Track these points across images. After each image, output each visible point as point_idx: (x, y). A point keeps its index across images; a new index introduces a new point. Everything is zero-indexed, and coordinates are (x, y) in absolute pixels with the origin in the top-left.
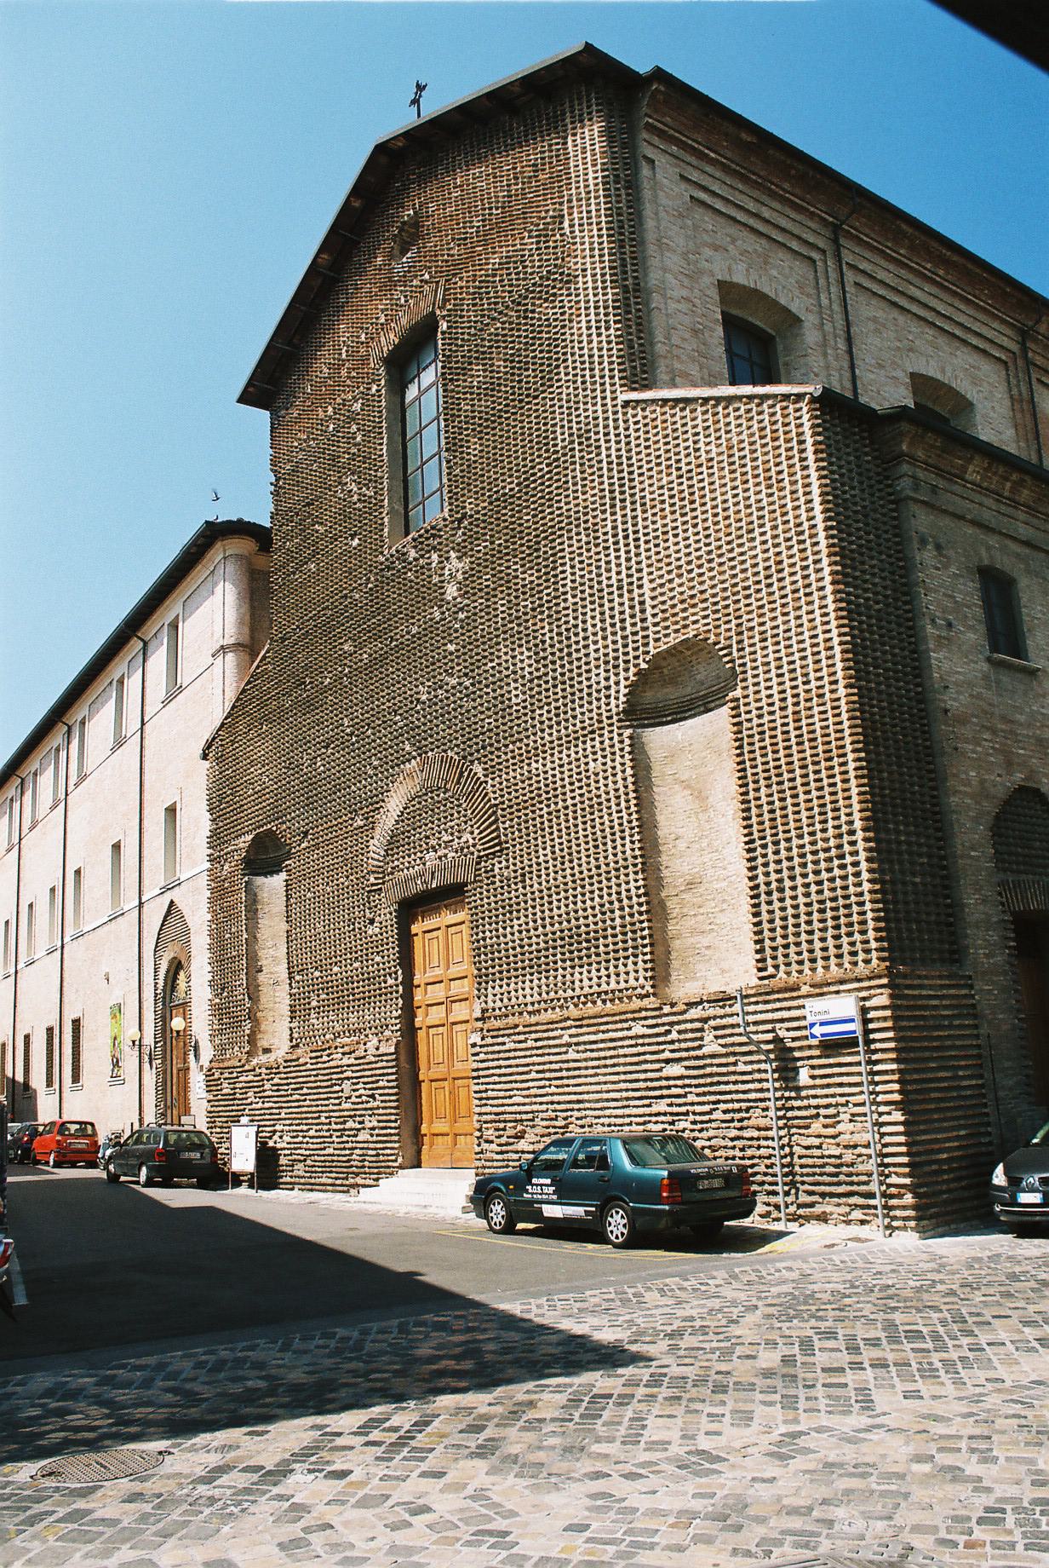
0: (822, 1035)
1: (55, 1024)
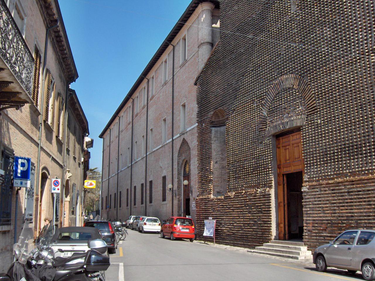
1: (107, 196)
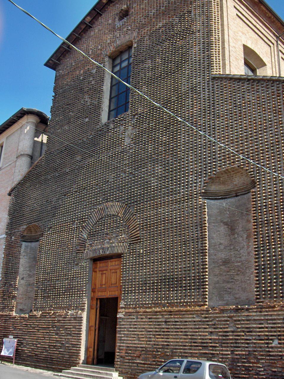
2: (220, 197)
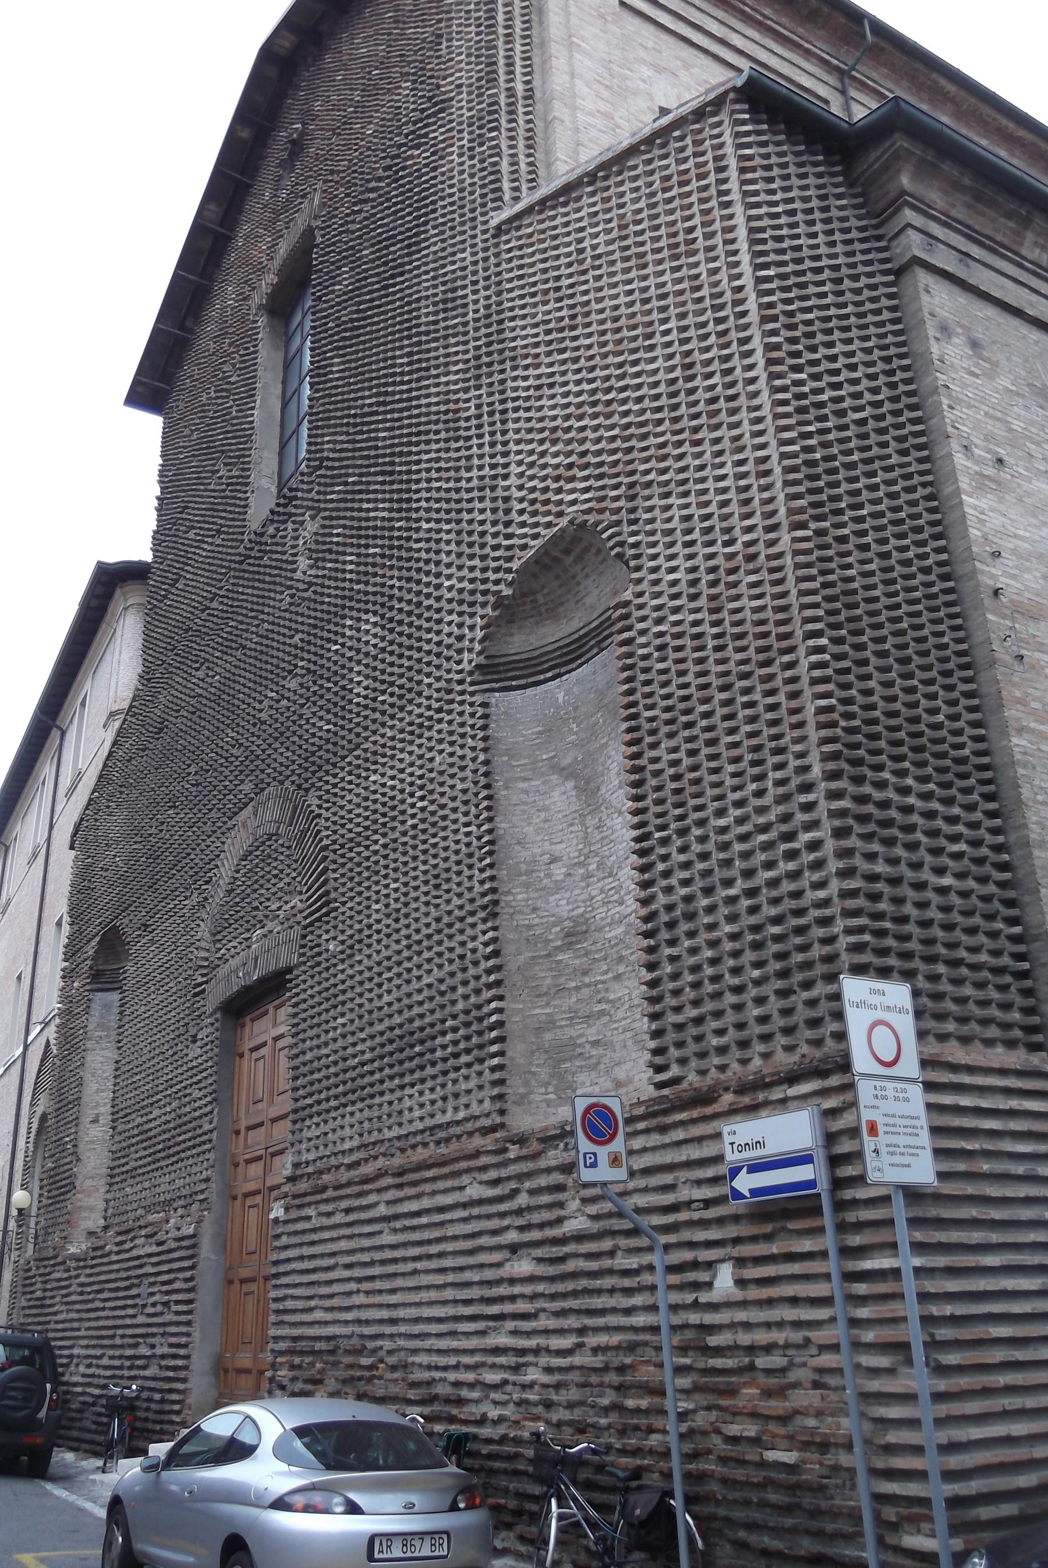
0: (754, 1192)
2: (549, 674)
